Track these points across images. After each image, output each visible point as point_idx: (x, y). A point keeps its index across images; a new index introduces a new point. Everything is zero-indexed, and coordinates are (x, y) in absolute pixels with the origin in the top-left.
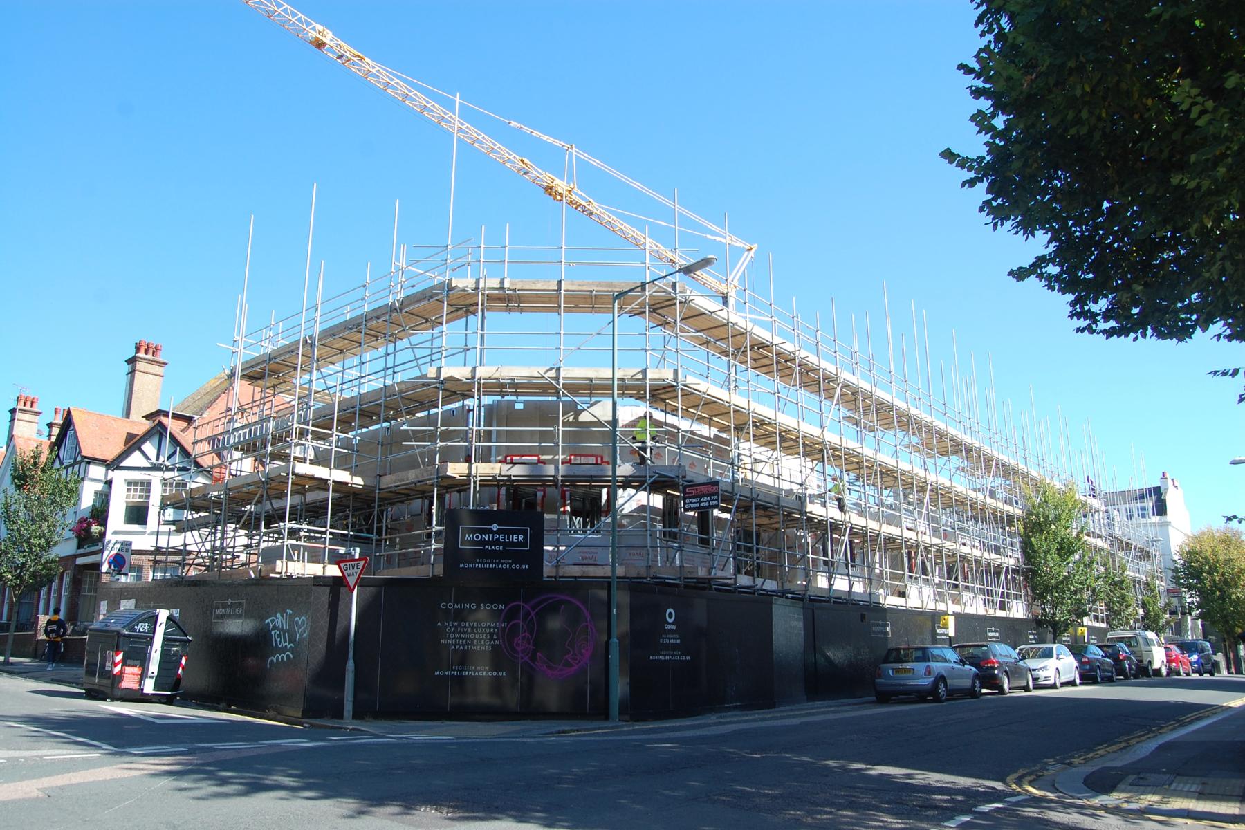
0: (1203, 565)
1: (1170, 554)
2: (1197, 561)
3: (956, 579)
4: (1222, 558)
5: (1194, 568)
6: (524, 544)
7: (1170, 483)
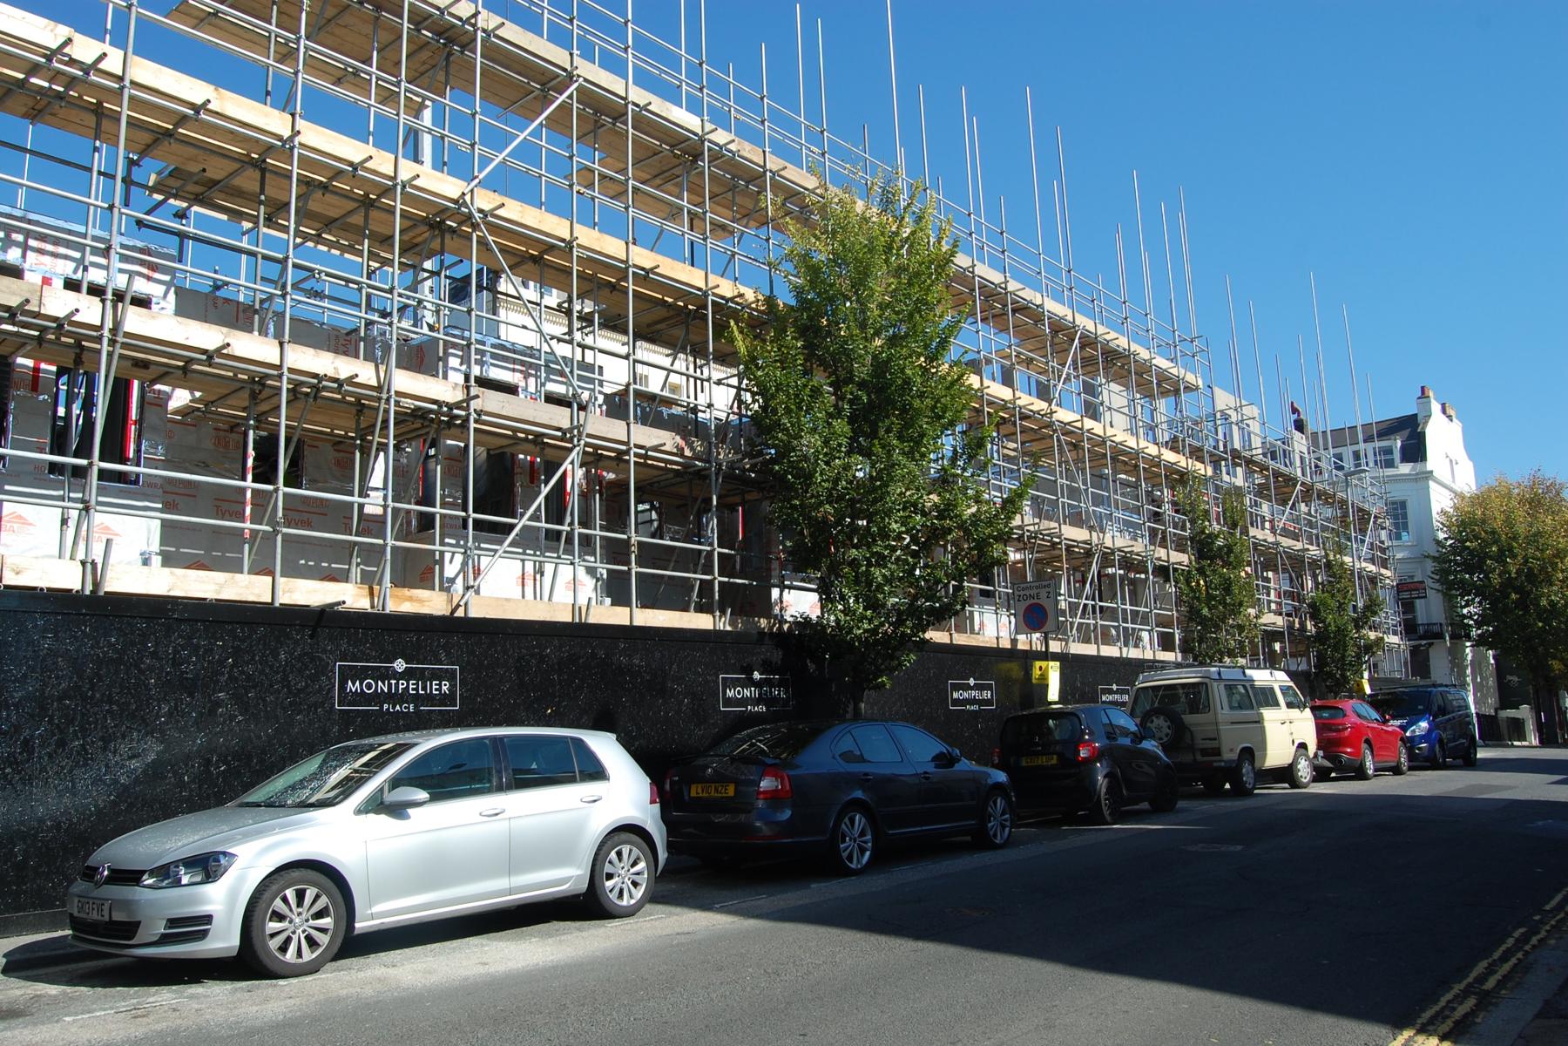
0: (1486, 544)
1: (1433, 531)
2: (1476, 537)
3: (428, 500)
4: (1521, 529)
5: (1471, 552)
6: (346, 675)
7: (1436, 407)
